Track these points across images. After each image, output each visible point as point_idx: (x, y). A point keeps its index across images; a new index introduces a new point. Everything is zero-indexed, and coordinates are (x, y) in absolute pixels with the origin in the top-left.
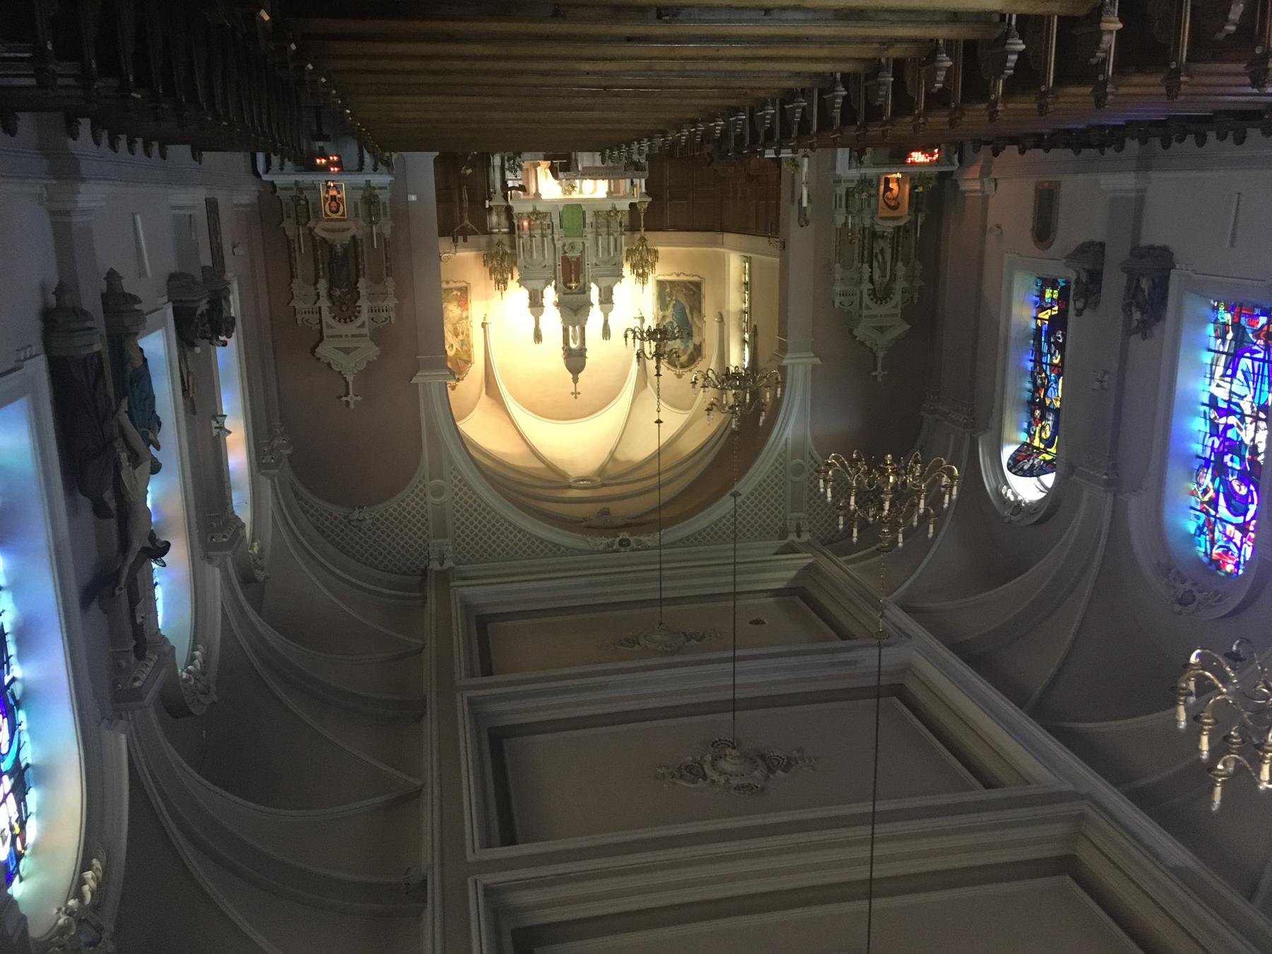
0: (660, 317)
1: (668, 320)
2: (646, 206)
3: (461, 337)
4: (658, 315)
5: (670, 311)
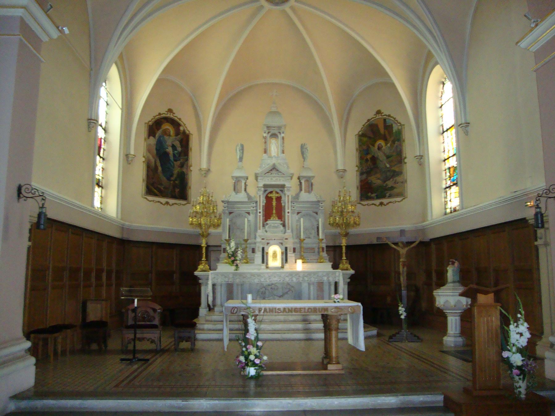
0: (185, 166)
1: (178, 163)
2: (201, 267)
3: (369, 157)
4: (187, 169)
5: (176, 171)
